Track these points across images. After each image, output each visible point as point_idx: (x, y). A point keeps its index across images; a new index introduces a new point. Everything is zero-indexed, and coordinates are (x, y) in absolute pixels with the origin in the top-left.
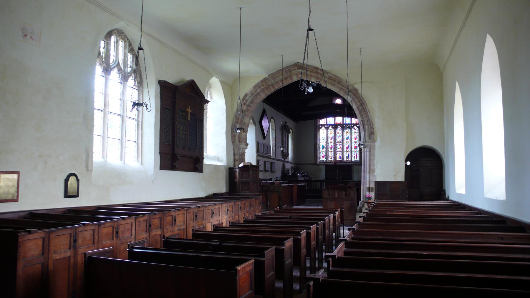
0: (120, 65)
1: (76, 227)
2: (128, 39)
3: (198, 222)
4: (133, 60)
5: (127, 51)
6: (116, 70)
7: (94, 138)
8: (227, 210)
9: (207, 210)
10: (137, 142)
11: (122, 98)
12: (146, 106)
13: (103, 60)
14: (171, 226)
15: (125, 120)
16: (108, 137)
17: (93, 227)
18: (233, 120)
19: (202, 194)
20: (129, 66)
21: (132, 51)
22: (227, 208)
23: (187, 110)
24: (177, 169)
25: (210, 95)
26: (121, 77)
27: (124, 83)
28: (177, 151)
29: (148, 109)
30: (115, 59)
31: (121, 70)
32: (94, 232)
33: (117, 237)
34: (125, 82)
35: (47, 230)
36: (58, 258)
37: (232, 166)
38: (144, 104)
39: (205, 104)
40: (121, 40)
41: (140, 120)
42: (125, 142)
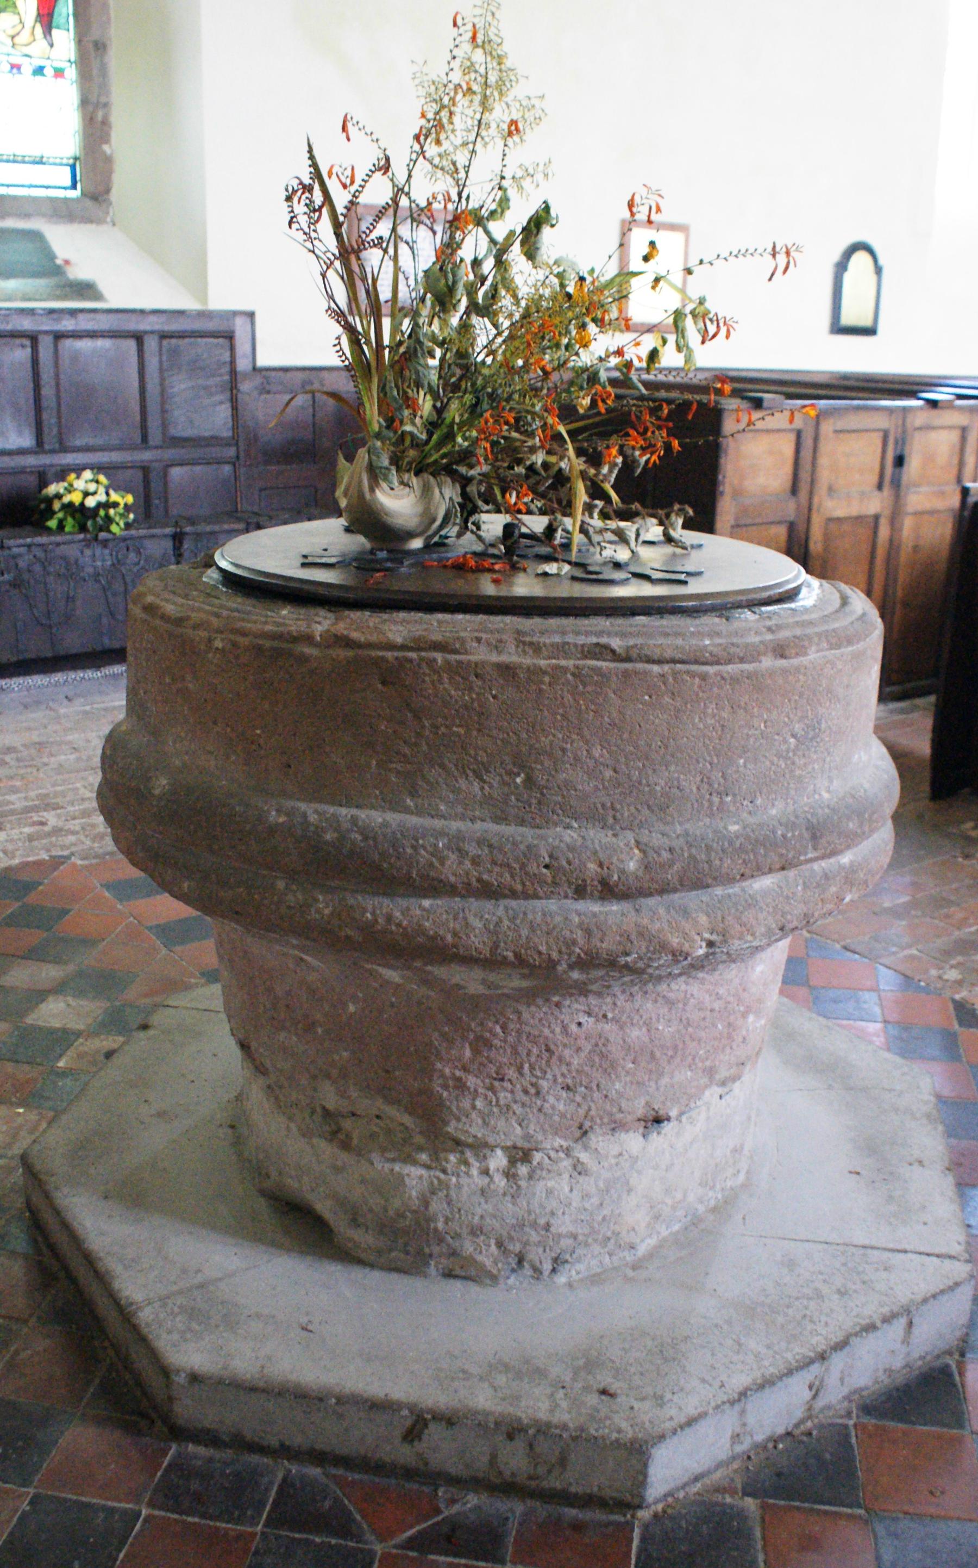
1: (905, 409)
32: (963, 439)
36: (840, 513)
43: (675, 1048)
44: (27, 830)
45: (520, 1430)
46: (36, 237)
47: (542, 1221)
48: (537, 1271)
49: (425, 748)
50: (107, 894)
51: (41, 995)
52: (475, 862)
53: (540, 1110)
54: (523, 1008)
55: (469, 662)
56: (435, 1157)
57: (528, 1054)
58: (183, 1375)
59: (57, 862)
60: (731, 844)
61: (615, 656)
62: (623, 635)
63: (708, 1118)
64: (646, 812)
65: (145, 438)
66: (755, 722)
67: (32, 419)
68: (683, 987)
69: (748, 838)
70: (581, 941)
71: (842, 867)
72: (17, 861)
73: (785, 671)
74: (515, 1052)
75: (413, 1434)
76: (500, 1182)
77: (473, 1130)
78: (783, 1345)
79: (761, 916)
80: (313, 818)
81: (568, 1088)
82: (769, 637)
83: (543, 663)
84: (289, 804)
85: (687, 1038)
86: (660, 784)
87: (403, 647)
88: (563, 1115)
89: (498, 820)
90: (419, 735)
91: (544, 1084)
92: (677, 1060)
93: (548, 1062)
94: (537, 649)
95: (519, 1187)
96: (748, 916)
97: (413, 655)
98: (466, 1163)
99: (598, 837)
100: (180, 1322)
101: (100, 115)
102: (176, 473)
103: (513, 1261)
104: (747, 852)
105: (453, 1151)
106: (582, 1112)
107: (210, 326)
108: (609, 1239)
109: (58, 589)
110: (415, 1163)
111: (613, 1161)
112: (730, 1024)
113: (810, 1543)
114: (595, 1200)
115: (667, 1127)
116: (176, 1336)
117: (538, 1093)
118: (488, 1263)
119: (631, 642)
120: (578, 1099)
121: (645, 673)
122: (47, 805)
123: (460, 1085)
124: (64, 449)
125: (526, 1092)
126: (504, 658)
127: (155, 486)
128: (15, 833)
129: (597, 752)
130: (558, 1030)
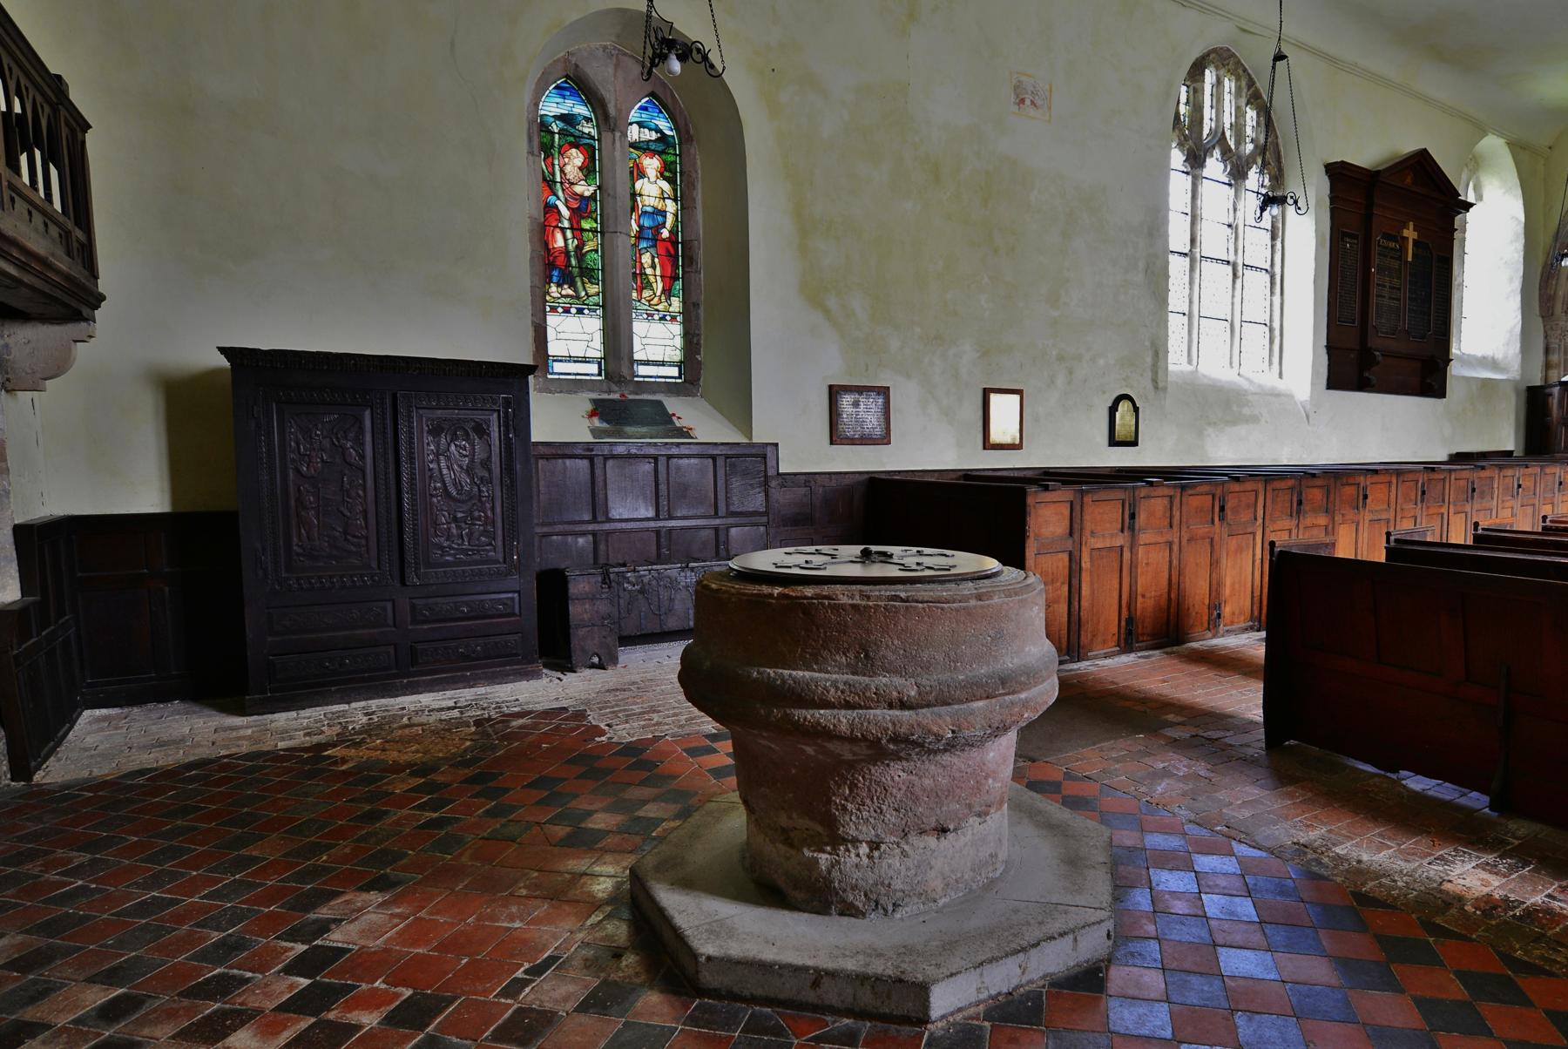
0: (1226, 139)
2: (1245, 70)
3: (1428, 508)
4: (1258, 123)
5: (1243, 101)
6: (1217, 153)
7: (1170, 319)
8: (1516, 486)
9: (1456, 479)
10: (1271, 325)
11: (1231, 220)
12: (1296, 202)
13: (1187, 132)
14: (1354, 509)
15: (1240, 274)
16: (1200, 317)
17: (1167, 491)
18: (1549, 254)
19: (1441, 455)
20: (1248, 140)
21: (1257, 99)
22: (1518, 480)
23: (1406, 233)
24: (1373, 386)
25: (1475, 189)
26: (1228, 170)
27: (1236, 183)
28: (1375, 342)
29: (1299, 208)
30: (1213, 126)
31: (1230, 150)
33: (1222, 519)
34: (1240, 181)
35: (1077, 487)
37: (1538, 382)
38: (1289, 198)
39: (1461, 213)
40: (1229, 75)
41: (1278, 270)
42: (1241, 326)
43: (949, 791)
44: (642, 723)
45: (867, 979)
46: (660, 403)
47: (886, 882)
48: (885, 910)
49: (821, 642)
50: (685, 754)
51: (645, 802)
52: (843, 692)
53: (883, 821)
54: (871, 767)
55: (839, 604)
56: (834, 849)
57: (876, 791)
58: (704, 957)
59: (656, 739)
60: (960, 684)
61: (902, 600)
62: (906, 591)
63: (973, 834)
64: (919, 669)
65: (716, 513)
66: (969, 629)
67: (654, 502)
68: (949, 759)
69: (968, 682)
70: (891, 728)
71: (1020, 700)
72: (635, 739)
73: (982, 607)
74: (869, 790)
75: (816, 984)
76: (865, 860)
77: (851, 832)
78: (1005, 944)
79: (978, 719)
80: (772, 675)
81: (896, 810)
82: (975, 592)
83: (871, 603)
84: (762, 669)
85: (954, 787)
86: (925, 656)
87: (812, 598)
88: (894, 825)
89: (853, 674)
90: (819, 637)
91: (884, 807)
92: (951, 797)
93: (886, 795)
94: (868, 598)
95: (874, 863)
96: (971, 718)
97: (816, 601)
98: (849, 851)
99: (898, 681)
100: (704, 936)
101: (695, 340)
102: (733, 531)
103: (873, 904)
104: (967, 688)
105: (842, 844)
106: (903, 822)
107: (754, 451)
108: (922, 894)
109: (664, 595)
110: (824, 851)
111: (922, 851)
112: (977, 782)
113: (1013, 1040)
114: (913, 872)
115: (950, 836)
116: (702, 941)
117: (881, 812)
118: (860, 905)
119: (910, 594)
120: (901, 816)
121: (916, 607)
122: (653, 710)
123: (844, 808)
124: (671, 518)
125: (875, 811)
126: (855, 602)
127: (722, 538)
128: (636, 725)
129: (896, 642)
130: (889, 779)
